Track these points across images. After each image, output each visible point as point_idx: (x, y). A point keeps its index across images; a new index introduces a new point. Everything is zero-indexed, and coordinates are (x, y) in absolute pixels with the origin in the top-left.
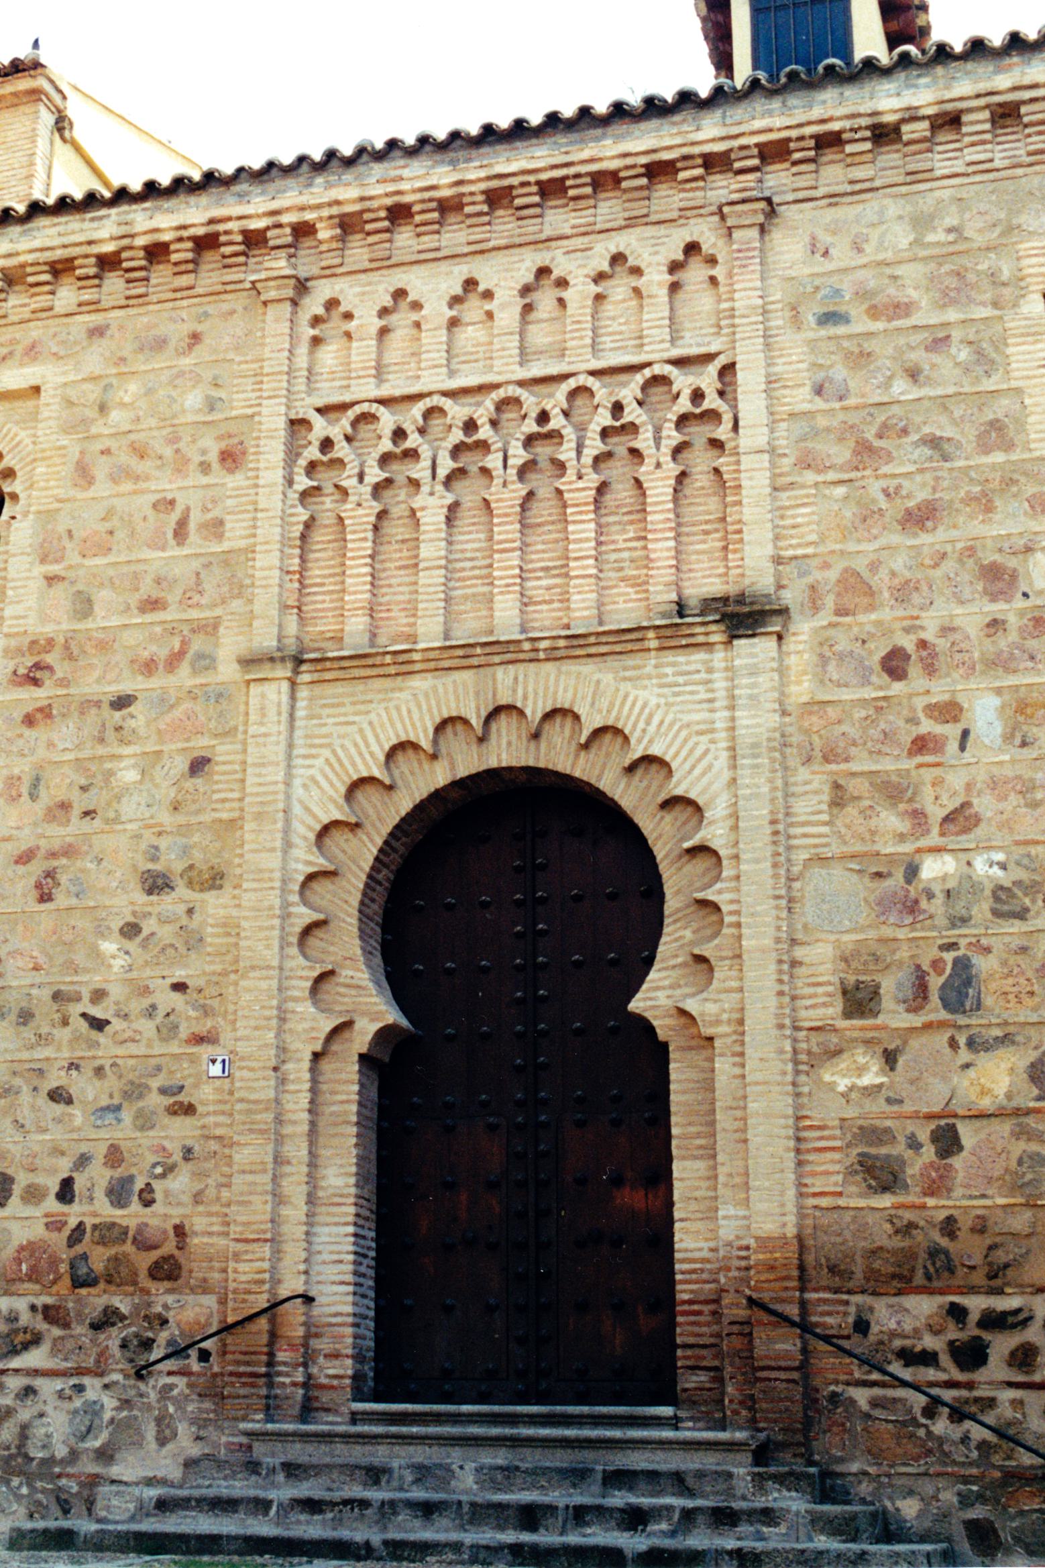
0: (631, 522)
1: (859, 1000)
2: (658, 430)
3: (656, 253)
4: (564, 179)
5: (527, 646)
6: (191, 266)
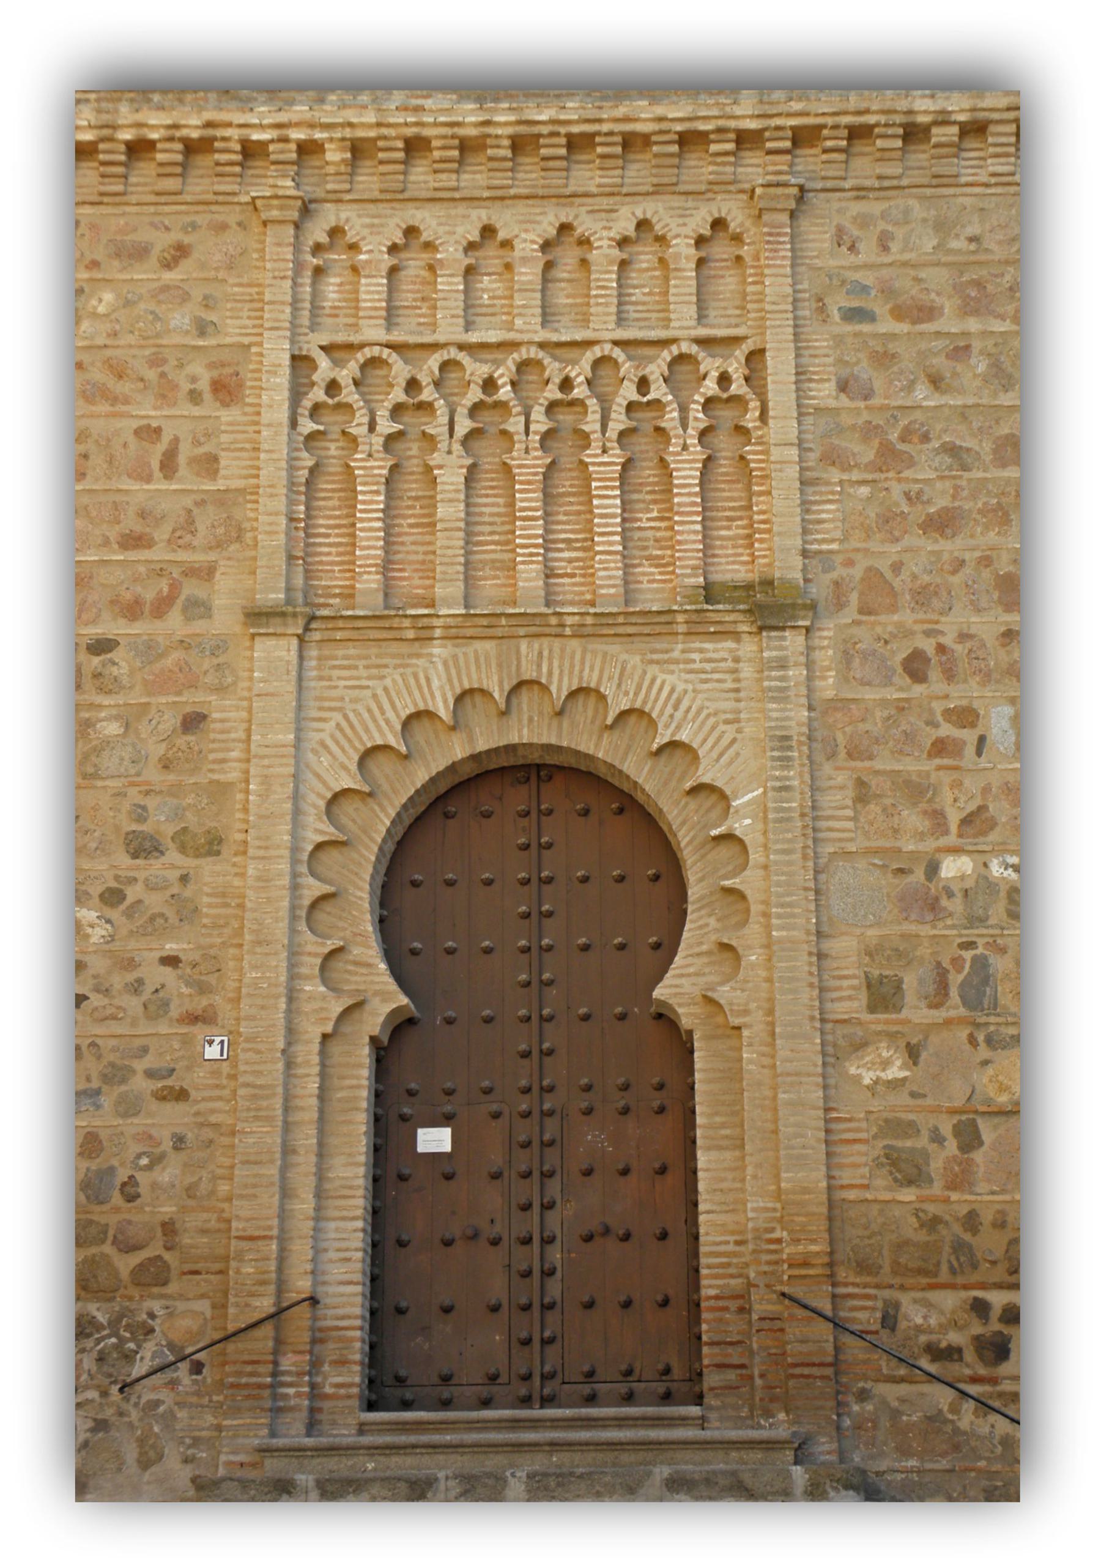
0: (655, 502)
1: (883, 995)
2: (683, 409)
3: (685, 225)
4: (594, 135)
5: (554, 621)
6: (179, 170)
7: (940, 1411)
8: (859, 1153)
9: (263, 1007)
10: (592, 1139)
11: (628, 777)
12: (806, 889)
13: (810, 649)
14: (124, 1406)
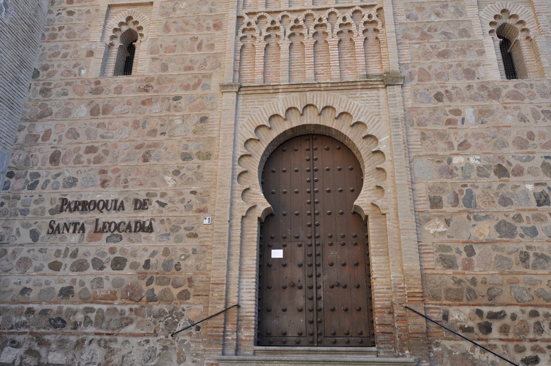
0: (349, 52)
1: (435, 203)
7: (467, 351)
8: (430, 257)
9: (222, 207)
10: (332, 254)
11: (343, 134)
12: (406, 167)
13: (403, 92)
14: (173, 341)
